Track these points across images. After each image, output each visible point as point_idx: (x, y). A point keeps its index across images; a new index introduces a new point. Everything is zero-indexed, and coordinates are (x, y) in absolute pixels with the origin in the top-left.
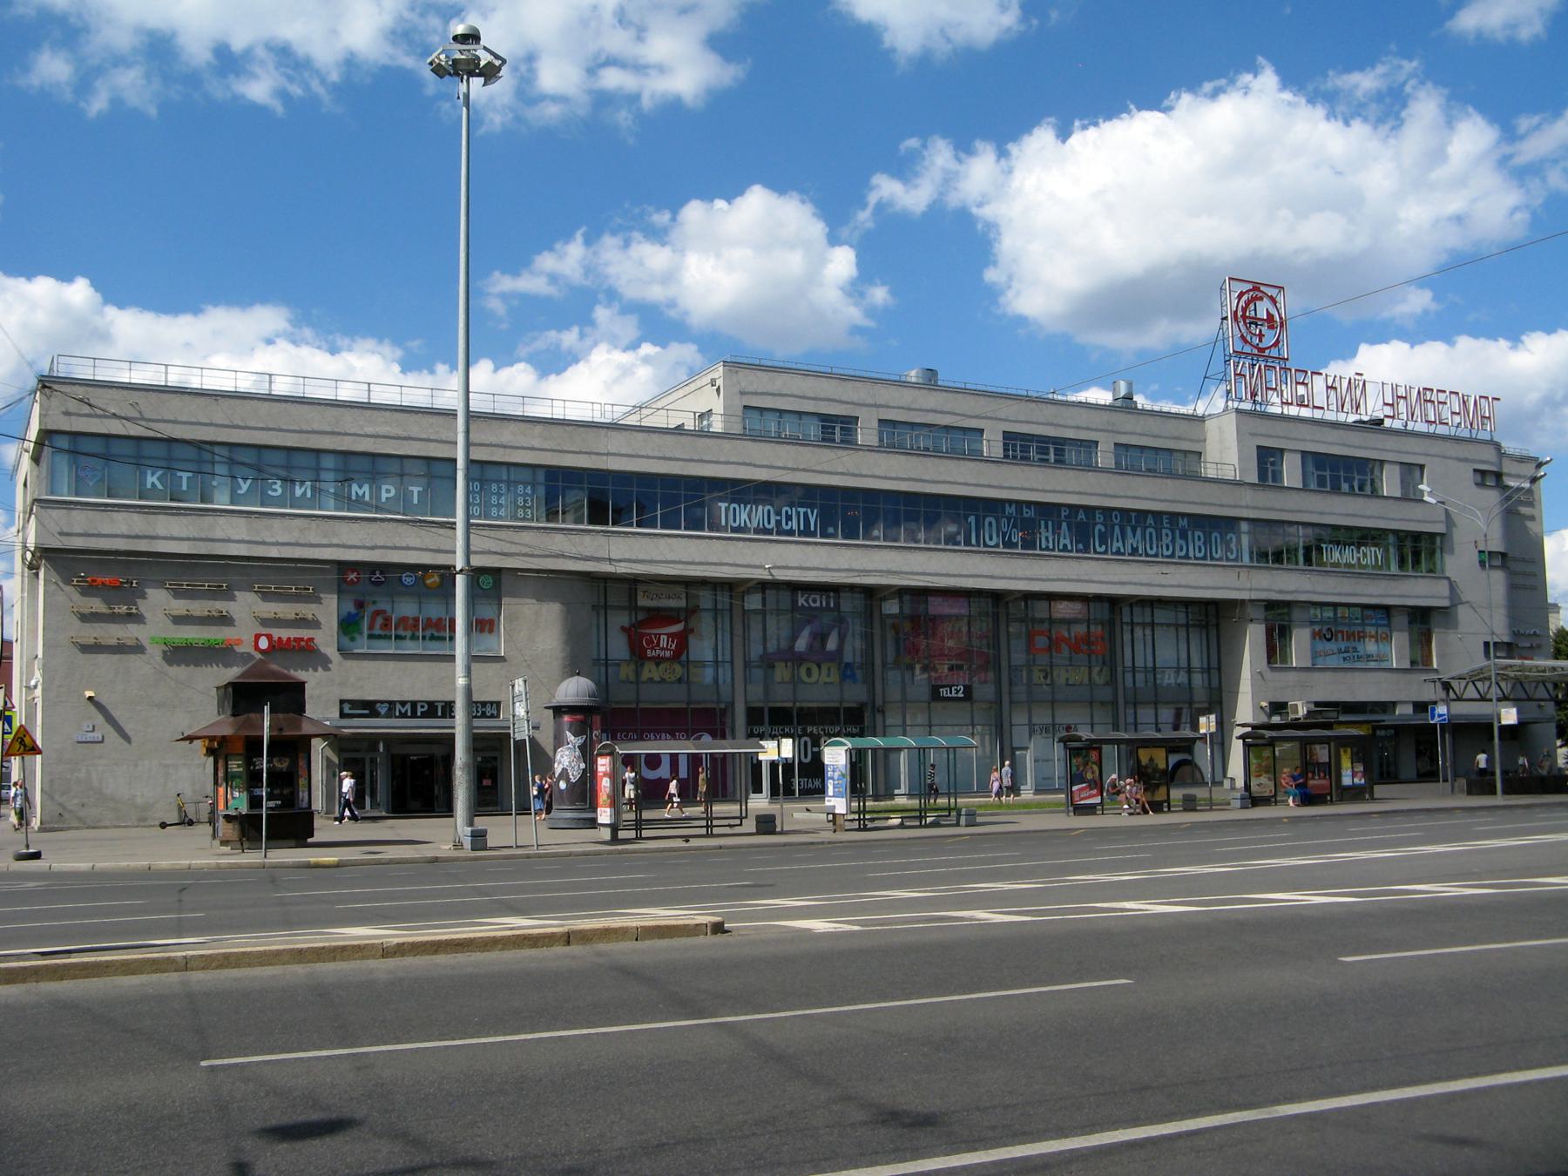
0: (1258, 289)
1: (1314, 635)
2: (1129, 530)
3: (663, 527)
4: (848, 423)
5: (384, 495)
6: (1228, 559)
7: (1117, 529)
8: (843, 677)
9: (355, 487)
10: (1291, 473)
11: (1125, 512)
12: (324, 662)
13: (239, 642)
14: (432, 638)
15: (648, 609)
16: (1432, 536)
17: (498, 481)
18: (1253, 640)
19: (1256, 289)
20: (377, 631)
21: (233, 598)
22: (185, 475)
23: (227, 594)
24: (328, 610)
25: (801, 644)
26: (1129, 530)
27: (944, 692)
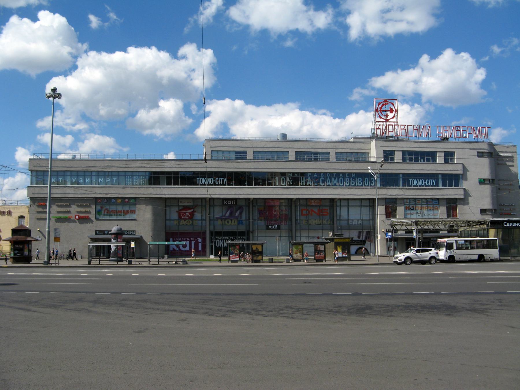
0: (386, 101)
1: (406, 209)
2: (333, 179)
3: (153, 185)
4: (245, 153)
5: (107, 181)
6: (371, 186)
7: (328, 179)
8: (239, 224)
9: (100, 179)
10: (398, 157)
11: (332, 174)
12: (92, 222)
13: (72, 217)
14: (119, 215)
15: (183, 206)
16: (457, 175)
17: (136, 176)
18: (381, 210)
19: (385, 101)
20: (106, 214)
21: (91, 207)
22: (115, 179)
23: (69, 206)
24: (93, 209)
25: (228, 214)
26: (333, 179)
27: (271, 227)
